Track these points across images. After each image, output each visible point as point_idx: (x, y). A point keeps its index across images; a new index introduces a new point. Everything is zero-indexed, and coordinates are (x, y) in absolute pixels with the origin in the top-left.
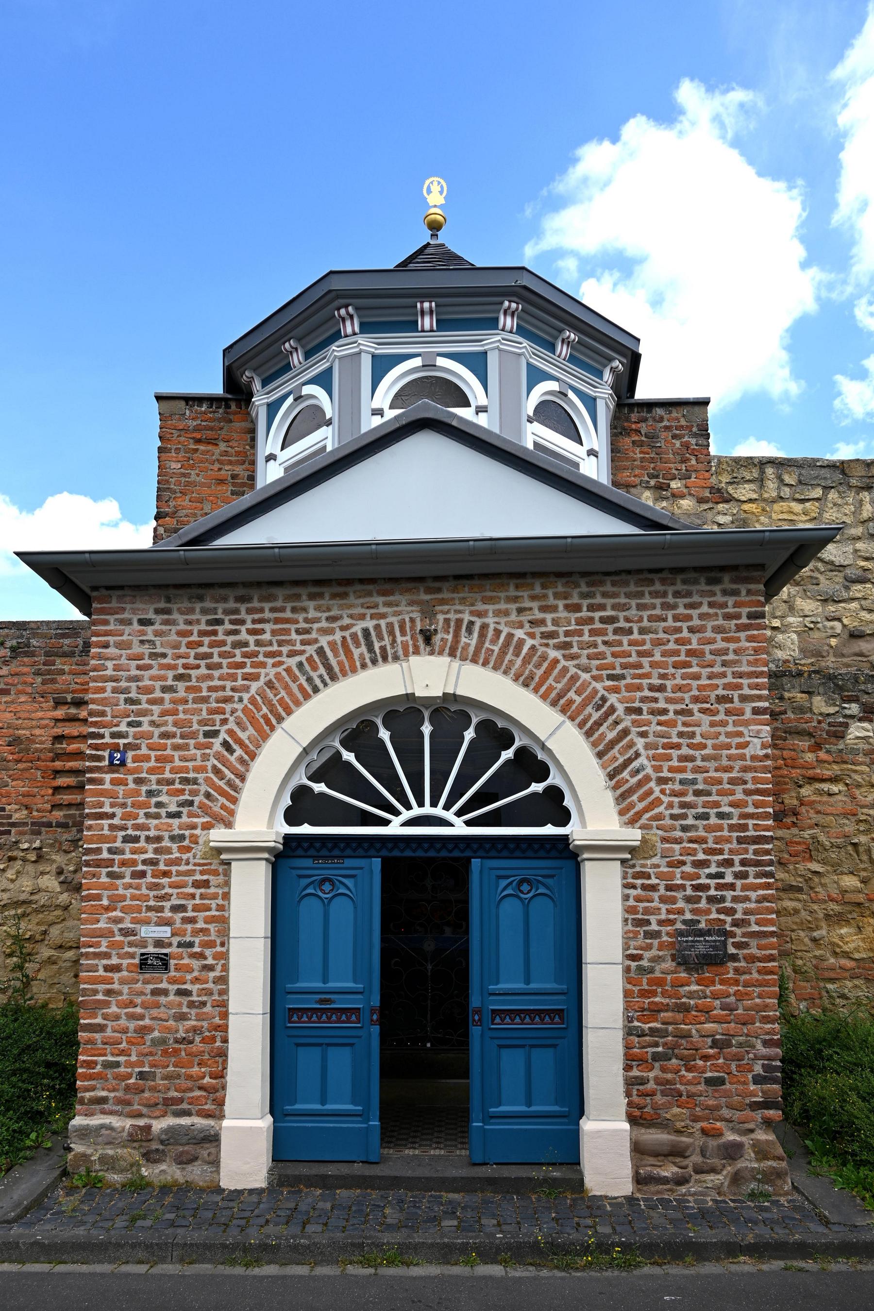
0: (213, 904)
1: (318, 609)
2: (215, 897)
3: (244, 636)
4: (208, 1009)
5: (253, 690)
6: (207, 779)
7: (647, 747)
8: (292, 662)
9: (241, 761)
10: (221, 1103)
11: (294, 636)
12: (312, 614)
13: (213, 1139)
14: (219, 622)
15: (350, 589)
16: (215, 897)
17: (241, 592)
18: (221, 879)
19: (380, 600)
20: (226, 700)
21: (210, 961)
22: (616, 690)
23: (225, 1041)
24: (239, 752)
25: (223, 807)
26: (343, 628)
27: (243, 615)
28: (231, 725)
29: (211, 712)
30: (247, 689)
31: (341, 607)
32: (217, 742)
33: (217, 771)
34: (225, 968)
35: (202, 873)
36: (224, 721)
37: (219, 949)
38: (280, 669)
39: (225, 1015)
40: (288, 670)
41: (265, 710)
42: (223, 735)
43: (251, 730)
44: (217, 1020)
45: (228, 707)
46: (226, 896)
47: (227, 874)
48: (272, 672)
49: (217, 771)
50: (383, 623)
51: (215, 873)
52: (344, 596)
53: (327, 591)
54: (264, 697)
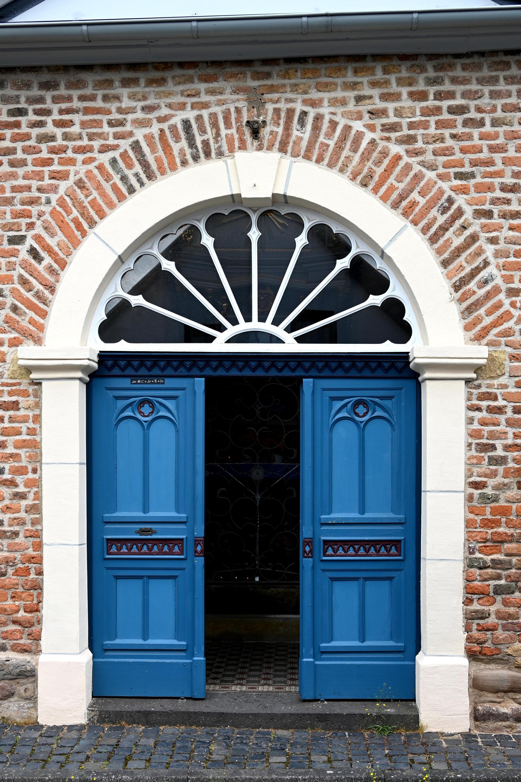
0: (24, 427)
1: (132, 97)
2: (25, 420)
3: (50, 128)
4: (21, 539)
5: (62, 191)
6: (13, 291)
7: (497, 254)
8: (105, 158)
9: (51, 270)
10: (37, 638)
11: (106, 128)
12: (126, 103)
13: (30, 675)
14: (22, 112)
15: (168, 74)
16: (25, 420)
17: (46, 77)
18: (31, 400)
19: (202, 87)
20: (33, 202)
21: (21, 489)
22: (464, 191)
23: (40, 573)
24: (48, 260)
25: (32, 321)
26: (161, 120)
27: (49, 104)
28: (39, 230)
29: (17, 215)
30: (54, 189)
31: (158, 95)
32: (23, 249)
33: (24, 282)
34: (38, 496)
35: (10, 394)
36: (31, 226)
37: (31, 476)
38: (91, 166)
39: (39, 546)
40: (100, 168)
41: (75, 213)
42: (30, 242)
43: (60, 236)
44: (31, 552)
45: (34, 210)
46: (37, 419)
47: (38, 395)
48: (82, 169)
49: (24, 282)
50: (205, 113)
51: (25, 394)
52: (161, 82)
53: (142, 77)
54: (74, 199)
